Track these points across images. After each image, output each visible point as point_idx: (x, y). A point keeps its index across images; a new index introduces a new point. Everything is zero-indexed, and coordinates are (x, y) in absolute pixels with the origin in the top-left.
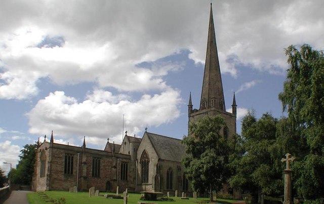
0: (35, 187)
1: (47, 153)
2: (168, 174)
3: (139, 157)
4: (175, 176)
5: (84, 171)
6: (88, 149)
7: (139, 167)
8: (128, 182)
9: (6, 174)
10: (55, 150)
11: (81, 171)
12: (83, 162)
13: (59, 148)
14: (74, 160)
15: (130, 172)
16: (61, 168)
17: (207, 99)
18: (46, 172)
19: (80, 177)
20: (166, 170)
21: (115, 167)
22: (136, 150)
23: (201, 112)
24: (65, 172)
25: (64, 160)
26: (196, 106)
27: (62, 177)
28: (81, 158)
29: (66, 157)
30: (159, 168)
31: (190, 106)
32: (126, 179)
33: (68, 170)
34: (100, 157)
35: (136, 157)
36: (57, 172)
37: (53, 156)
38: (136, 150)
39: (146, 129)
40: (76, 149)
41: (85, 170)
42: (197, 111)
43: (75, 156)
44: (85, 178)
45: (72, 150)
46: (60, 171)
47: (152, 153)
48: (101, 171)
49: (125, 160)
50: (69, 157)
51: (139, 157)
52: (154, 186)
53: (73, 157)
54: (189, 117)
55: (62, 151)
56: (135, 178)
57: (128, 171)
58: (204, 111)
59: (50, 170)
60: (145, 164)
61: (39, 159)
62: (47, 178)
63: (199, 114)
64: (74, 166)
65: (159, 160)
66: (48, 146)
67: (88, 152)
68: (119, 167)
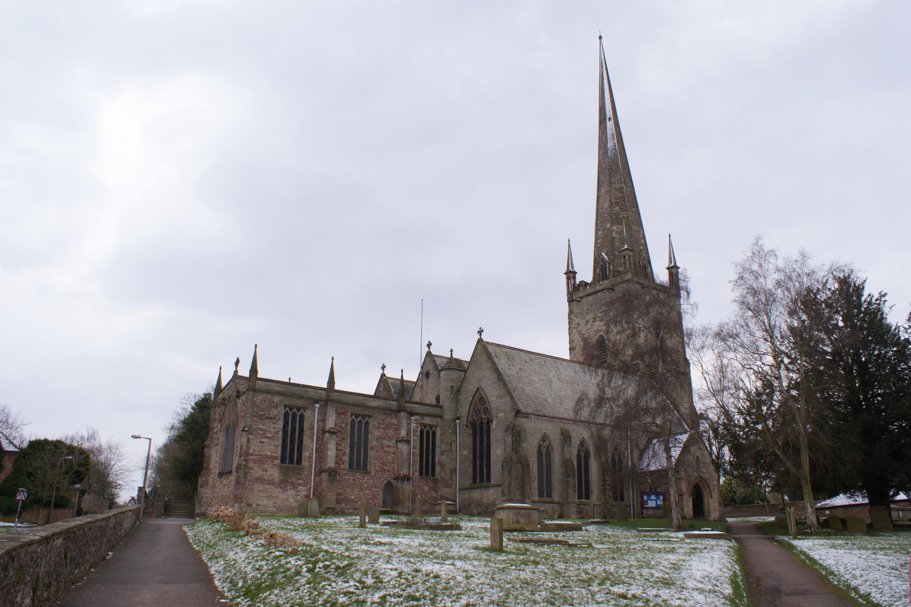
2: (539, 452)
4: (556, 459)
5: (329, 453)
11: (321, 451)
12: (327, 428)
14: (306, 425)
19: (319, 473)
20: (536, 443)
24: (283, 460)
25: (280, 425)
26: (585, 274)
27: (275, 473)
29: (286, 415)
31: (571, 274)
32: (433, 474)
34: (366, 412)
36: (262, 460)
41: (332, 453)
43: (307, 414)
48: (371, 453)
49: (428, 421)
50: (294, 415)
53: (302, 416)
54: (570, 301)
55: (277, 399)
57: (438, 451)
63: (594, 293)
67: (339, 402)
68: (415, 440)
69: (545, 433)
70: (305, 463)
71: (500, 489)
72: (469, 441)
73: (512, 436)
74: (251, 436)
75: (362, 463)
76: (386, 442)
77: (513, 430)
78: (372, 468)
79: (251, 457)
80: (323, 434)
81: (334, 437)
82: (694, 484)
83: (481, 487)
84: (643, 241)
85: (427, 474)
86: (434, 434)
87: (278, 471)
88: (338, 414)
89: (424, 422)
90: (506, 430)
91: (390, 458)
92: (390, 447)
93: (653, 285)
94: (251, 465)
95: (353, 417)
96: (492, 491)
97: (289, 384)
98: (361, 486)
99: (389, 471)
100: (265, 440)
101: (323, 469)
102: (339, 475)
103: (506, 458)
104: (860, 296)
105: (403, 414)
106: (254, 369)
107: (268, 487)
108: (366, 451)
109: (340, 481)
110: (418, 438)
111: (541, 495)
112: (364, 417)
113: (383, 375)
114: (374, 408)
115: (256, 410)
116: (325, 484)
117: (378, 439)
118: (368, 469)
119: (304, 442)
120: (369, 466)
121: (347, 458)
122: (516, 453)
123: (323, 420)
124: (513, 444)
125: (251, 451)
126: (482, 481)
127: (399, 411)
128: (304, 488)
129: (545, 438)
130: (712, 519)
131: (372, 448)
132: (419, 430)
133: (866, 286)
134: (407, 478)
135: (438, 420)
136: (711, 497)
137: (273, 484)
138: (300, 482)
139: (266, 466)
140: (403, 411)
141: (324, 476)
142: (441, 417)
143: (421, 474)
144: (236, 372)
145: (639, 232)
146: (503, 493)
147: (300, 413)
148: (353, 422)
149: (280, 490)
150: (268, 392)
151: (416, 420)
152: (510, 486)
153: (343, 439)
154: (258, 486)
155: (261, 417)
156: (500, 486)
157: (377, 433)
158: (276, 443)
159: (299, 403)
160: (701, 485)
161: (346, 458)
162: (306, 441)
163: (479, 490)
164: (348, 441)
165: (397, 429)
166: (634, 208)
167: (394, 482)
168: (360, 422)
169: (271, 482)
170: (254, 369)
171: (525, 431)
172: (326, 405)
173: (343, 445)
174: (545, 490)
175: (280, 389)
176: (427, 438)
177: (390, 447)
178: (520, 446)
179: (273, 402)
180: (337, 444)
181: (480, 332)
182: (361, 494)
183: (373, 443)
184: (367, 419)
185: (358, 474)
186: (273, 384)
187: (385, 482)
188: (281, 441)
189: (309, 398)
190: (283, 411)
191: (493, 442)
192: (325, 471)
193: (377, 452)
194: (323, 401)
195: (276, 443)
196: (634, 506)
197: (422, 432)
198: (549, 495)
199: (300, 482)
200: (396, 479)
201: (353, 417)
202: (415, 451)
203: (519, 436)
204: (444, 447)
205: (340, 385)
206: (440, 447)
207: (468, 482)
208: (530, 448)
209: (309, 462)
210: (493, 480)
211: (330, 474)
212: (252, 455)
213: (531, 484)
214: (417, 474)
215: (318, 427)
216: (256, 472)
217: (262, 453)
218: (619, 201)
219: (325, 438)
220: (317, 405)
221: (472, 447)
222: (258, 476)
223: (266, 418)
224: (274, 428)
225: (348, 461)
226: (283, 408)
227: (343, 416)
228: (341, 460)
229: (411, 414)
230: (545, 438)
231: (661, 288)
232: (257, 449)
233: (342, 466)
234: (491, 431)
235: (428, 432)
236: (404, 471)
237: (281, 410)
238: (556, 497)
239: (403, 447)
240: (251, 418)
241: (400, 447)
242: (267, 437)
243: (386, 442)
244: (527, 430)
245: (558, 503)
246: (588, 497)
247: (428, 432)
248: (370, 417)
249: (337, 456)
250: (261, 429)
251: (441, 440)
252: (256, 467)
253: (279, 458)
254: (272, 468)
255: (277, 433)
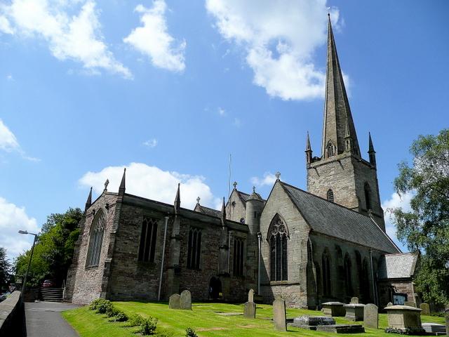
0: (70, 290)
1: (110, 216)
3: (265, 228)
6: (182, 208)
7: (265, 250)
9: (11, 258)
12: (174, 235)
13: (133, 205)
15: (248, 258)
16: (133, 248)
17: (336, 140)
18: (104, 258)
19: (166, 269)
21: (226, 248)
22: (257, 215)
23: (329, 160)
24: (140, 259)
25: (140, 231)
27: (133, 268)
28: (171, 225)
29: (144, 223)
30: (312, 249)
31: (309, 152)
33: (146, 258)
35: (259, 228)
36: (125, 257)
37: (123, 221)
38: (257, 215)
39: (198, 199)
40: (164, 209)
42: (319, 159)
43: (160, 224)
44: (178, 270)
45: (155, 210)
46: (130, 255)
47: (295, 219)
51: (265, 228)
52: (305, 288)
53: (156, 226)
56: (256, 271)
58: (333, 158)
59: (113, 252)
60: (279, 244)
61: (87, 231)
62: (105, 271)
64: (158, 243)
65: (312, 232)
66: (112, 201)
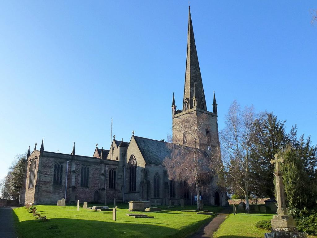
2: (155, 180)
4: (161, 182)
5: (73, 180)
8: (116, 190)
10: (45, 159)
11: (69, 179)
14: (63, 170)
19: (69, 187)
21: (103, 175)
25: (53, 169)
27: (51, 188)
29: (55, 166)
32: (115, 188)
36: (46, 183)
41: (73, 180)
43: (64, 165)
48: (90, 180)
49: (113, 167)
53: (62, 166)
55: (52, 159)
68: (107, 174)
69: (157, 172)
70: (63, 184)
71: (139, 193)
72: (128, 175)
73: (144, 173)
74: (41, 174)
75: (86, 184)
76: (96, 175)
77: (144, 171)
78: (90, 185)
79: (41, 182)
80: (70, 173)
81: (74, 174)
82: (215, 192)
83: (132, 193)
84: (203, 94)
85: (112, 187)
86: (115, 172)
87: (52, 188)
88: (76, 165)
89: (111, 167)
90: (142, 171)
91: (97, 182)
92: (97, 177)
93: (206, 112)
94: (41, 185)
95: (83, 166)
96: (136, 194)
97: (58, 153)
98: (86, 192)
99: (97, 187)
100: (46, 175)
101: (70, 186)
102: (77, 188)
103: (141, 182)
104: (274, 122)
105: (102, 164)
106: (42, 148)
107: (47, 194)
108: (88, 179)
109: (77, 191)
110: (108, 174)
111: (155, 195)
112: (87, 166)
113: (97, 148)
114: (91, 162)
115: (43, 164)
116: (71, 192)
117: (93, 174)
118: (88, 186)
119: (63, 176)
120: (89, 185)
121: (80, 182)
122: (145, 180)
123: (70, 168)
124: (144, 177)
125: (41, 180)
126: (133, 190)
127: (101, 163)
128: (62, 194)
129: (157, 174)
130: (222, 205)
131: (90, 178)
132: (109, 171)
133: (277, 118)
134: (104, 189)
135: (117, 166)
136: (223, 197)
137: (50, 193)
138: (61, 191)
139: (47, 186)
140: (103, 163)
141: (71, 189)
142: (118, 165)
143: (110, 187)
144: (35, 149)
145: (201, 90)
146: (140, 195)
147: (61, 165)
148: (82, 168)
149: (53, 195)
150: (48, 157)
151: (108, 167)
152: (142, 193)
153: (78, 174)
154: (44, 193)
155: (45, 167)
156: (139, 192)
157: (92, 172)
158: (51, 177)
159: (61, 161)
160: (219, 192)
161: (80, 182)
162: (64, 175)
163: (132, 194)
164: (81, 175)
165: (100, 170)
166: (200, 80)
167: (99, 191)
168: (85, 168)
169: (49, 192)
170: (42, 148)
171: (149, 171)
172: (72, 161)
173: (78, 177)
174: (157, 195)
175: (53, 156)
176: (112, 174)
177: (97, 177)
178: (147, 177)
179: (50, 161)
180: (76, 177)
181: (97, 145)
182: (86, 196)
183: (90, 176)
184: (88, 166)
185: (84, 188)
186: (50, 154)
187: (95, 191)
188: (53, 176)
189: (65, 159)
190: (54, 164)
191: (137, 175)
192: (71, 187)
193: (92, 179)
194: (70, 160)
195: (51, 177)
196: (192, 200)
197: (110, 171)
198: (159, 196)
199: (61, 191)
200: (100, 189)
201: (83, 166)
202: (108, 179)
203: (146, 173)
204: (119, 177)
205: (77, 153)
206: (117, 177)
207: (128, 191)
208: (151, 177)
209: (65, 184)
210: (137, 190)
211: (73, 189)
212: (41, 181)
213: (151, 191)
214: (108, 188)
215: (68, 170)
216: (44, 188)
217: (45, 181)
218: (194, 77)
219: (71, 174)
220: (68, 162)
221: (129, 177)
222: (43, 189)
223: (47, 167)
224: (50, 171)
225: (80, 183)
226: (54, 163)
227: (78, 166)
228: (77, 183)
229: (106, 164)
230: (157, 174)
231: (209, 113)
232: (43, 179)
233: (78, 185)
234: (137, 171)
235: (113, 171)
236: (103, 187)
237: (53, 164)
238: (161, 197)
239: (102, 177)
240: (41, 167)
241: (101, 177)
242: (48, 174)
243: (96, 175)
244: (150, 171)
245: (162, 199)
246: (174, 197)
247: (113, 171)
248: (89, 166)
249: (76, 181)
250: (45, 171)
251: (118, 174)
252: (43, 186)
253: (52, 183)
254: (49, 186)
255: (51, 173)
